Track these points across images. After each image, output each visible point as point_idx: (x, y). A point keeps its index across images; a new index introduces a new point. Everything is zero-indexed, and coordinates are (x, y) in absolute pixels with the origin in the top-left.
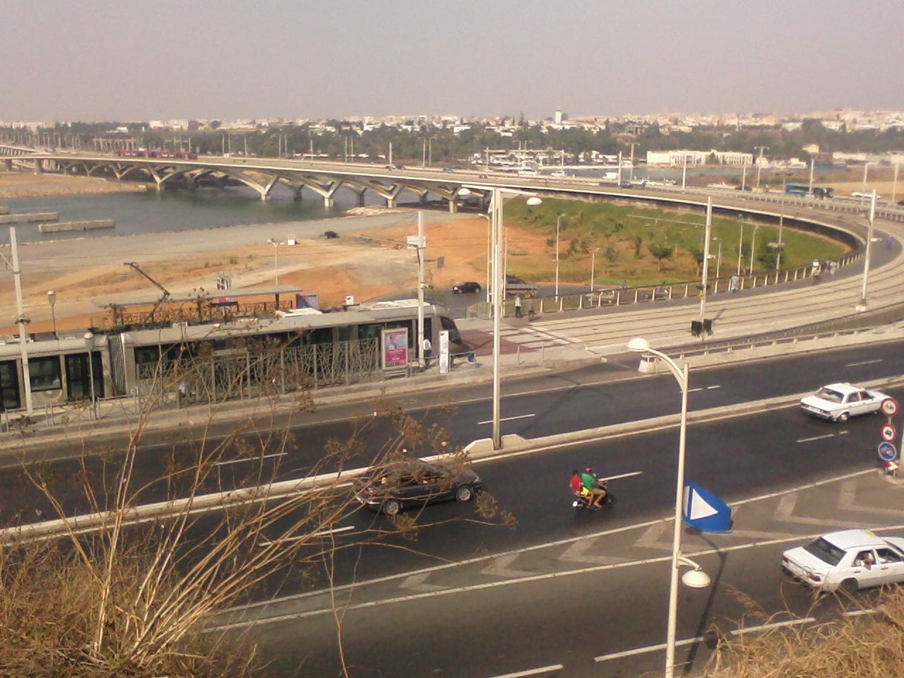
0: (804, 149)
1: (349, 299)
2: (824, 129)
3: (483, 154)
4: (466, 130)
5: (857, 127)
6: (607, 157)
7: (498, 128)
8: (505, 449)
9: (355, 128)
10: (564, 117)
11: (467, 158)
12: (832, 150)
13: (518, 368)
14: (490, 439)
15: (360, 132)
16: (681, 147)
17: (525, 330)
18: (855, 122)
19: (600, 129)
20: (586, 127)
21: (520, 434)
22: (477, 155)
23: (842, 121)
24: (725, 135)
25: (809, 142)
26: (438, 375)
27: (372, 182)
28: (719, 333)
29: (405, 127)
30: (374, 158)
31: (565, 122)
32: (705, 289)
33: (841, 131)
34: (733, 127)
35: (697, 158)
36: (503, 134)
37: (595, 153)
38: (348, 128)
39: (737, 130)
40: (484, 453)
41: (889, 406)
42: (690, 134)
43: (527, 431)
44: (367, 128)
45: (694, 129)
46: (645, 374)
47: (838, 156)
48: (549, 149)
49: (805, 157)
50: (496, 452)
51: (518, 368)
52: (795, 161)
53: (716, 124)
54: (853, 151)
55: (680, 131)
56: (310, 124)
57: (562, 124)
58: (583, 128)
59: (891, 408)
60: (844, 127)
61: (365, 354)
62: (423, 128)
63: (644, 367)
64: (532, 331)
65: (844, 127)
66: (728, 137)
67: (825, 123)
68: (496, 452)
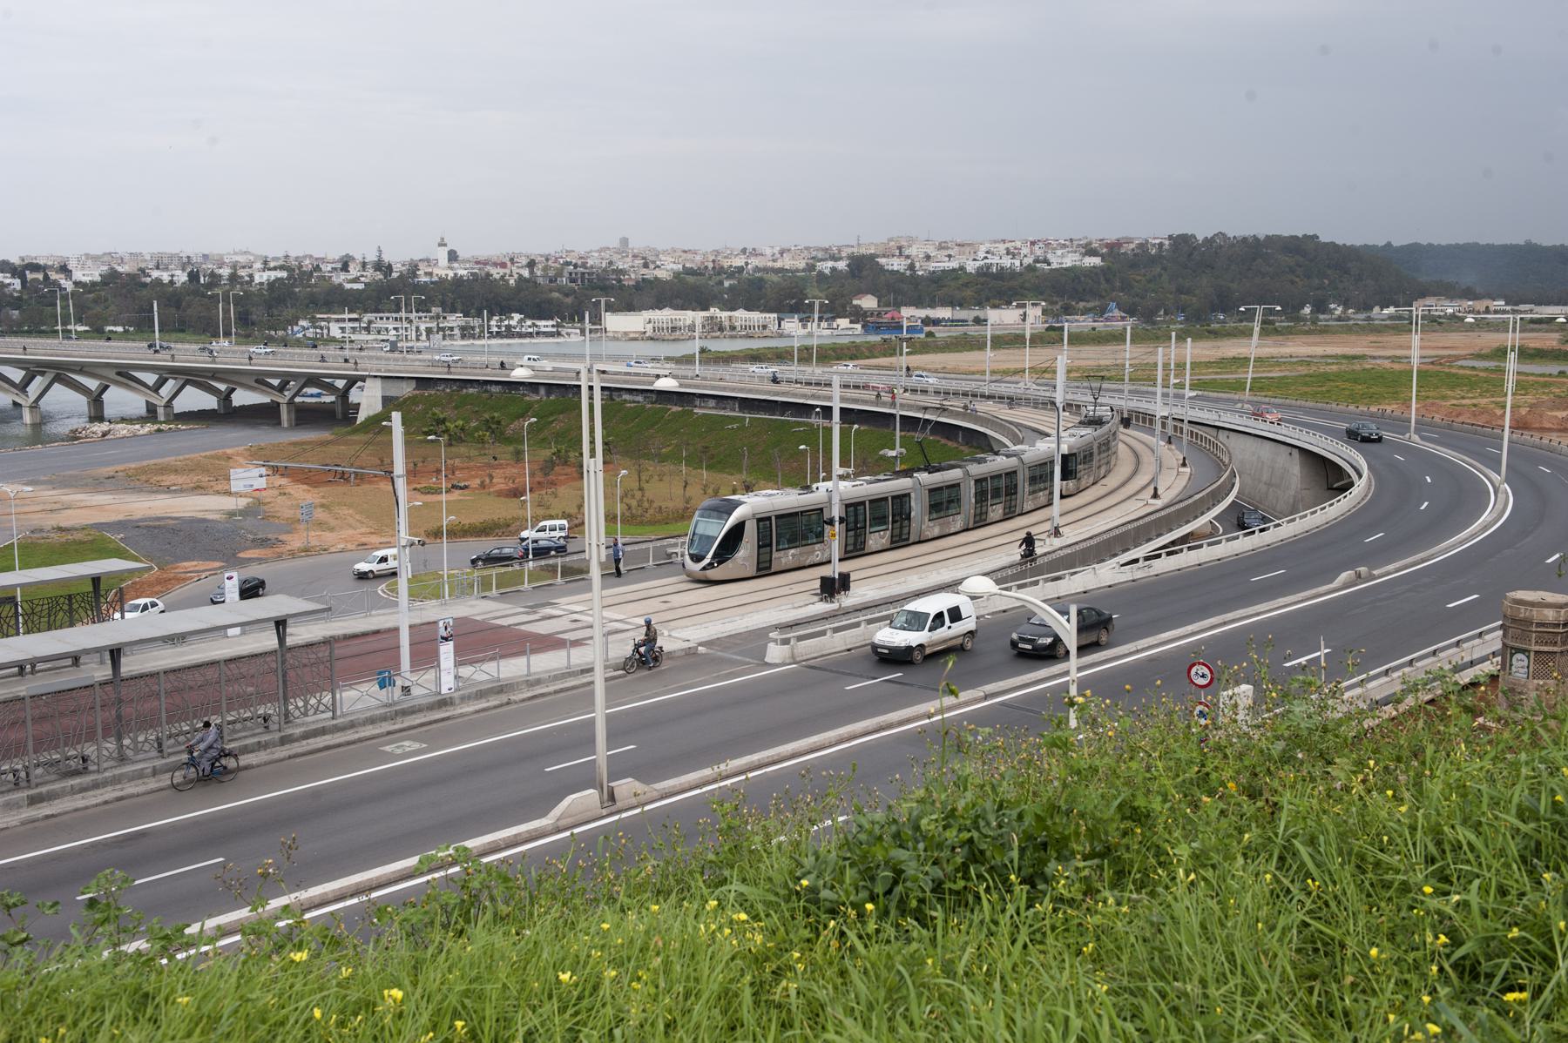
0: (855, 302)
1: (230, 578)
2: (881, 268)
3: (313, 320)
4: (278, 279)
5: (932, 266)
6: (538, 323)
7: (338, 277)
8: (619, 805)
9: (53, 276)
10: (453, 256)
11: (285, 329)
12: (898, 305)
13: (384, 718)
14: (591, 791)
15: (68, 286)
16: (659, 305)
17: (548, 611)
18: (928, 257)
19: (520, 276)
20: (496, 273)
21: (638, 778)
22: (303, 323)
23: (908, 257)
24: (727, 284)
25: (861, 292)
26: (439, 698)
27: (119, 374)
28: (859, 594)
29: (155, 274)
30: (98, 332)
31: (456, 265)
32: (837, 524)
33: (908, 273)
34: (740, 270)
35: (689, 322)
36: (348, 286)
37: (517, 317)
38: (40, 276)
39: (395, 275)
40: (589, 815)
41: (1200, 673)
42: (667, 282)
43: (647, 770)
44: (78, 275)
45: (677, 275)
46: (776, 665)
47: (910, 314)
48: (436, 310)
49: (858, 315)
50: (604, 812)
51: (384, 718)
52: (843, 323)
53: (711, 265)
54: (932, 306)
55: (656, 278)
56: (878, 256)
57: (452, 268)
58: (488, 275)
59: (1203, 676)
60: (912, 267)
61: (127, 710)
62: (193, 276)
63: (775, 652)
64: (561, 613)
65: (912, 267)
66: (731, 288)
67: (882, 261)
68: (604, 812)
